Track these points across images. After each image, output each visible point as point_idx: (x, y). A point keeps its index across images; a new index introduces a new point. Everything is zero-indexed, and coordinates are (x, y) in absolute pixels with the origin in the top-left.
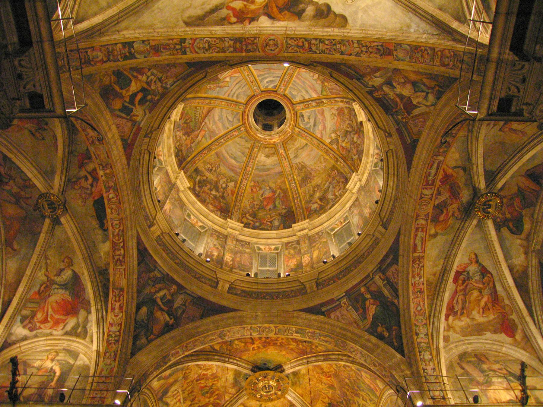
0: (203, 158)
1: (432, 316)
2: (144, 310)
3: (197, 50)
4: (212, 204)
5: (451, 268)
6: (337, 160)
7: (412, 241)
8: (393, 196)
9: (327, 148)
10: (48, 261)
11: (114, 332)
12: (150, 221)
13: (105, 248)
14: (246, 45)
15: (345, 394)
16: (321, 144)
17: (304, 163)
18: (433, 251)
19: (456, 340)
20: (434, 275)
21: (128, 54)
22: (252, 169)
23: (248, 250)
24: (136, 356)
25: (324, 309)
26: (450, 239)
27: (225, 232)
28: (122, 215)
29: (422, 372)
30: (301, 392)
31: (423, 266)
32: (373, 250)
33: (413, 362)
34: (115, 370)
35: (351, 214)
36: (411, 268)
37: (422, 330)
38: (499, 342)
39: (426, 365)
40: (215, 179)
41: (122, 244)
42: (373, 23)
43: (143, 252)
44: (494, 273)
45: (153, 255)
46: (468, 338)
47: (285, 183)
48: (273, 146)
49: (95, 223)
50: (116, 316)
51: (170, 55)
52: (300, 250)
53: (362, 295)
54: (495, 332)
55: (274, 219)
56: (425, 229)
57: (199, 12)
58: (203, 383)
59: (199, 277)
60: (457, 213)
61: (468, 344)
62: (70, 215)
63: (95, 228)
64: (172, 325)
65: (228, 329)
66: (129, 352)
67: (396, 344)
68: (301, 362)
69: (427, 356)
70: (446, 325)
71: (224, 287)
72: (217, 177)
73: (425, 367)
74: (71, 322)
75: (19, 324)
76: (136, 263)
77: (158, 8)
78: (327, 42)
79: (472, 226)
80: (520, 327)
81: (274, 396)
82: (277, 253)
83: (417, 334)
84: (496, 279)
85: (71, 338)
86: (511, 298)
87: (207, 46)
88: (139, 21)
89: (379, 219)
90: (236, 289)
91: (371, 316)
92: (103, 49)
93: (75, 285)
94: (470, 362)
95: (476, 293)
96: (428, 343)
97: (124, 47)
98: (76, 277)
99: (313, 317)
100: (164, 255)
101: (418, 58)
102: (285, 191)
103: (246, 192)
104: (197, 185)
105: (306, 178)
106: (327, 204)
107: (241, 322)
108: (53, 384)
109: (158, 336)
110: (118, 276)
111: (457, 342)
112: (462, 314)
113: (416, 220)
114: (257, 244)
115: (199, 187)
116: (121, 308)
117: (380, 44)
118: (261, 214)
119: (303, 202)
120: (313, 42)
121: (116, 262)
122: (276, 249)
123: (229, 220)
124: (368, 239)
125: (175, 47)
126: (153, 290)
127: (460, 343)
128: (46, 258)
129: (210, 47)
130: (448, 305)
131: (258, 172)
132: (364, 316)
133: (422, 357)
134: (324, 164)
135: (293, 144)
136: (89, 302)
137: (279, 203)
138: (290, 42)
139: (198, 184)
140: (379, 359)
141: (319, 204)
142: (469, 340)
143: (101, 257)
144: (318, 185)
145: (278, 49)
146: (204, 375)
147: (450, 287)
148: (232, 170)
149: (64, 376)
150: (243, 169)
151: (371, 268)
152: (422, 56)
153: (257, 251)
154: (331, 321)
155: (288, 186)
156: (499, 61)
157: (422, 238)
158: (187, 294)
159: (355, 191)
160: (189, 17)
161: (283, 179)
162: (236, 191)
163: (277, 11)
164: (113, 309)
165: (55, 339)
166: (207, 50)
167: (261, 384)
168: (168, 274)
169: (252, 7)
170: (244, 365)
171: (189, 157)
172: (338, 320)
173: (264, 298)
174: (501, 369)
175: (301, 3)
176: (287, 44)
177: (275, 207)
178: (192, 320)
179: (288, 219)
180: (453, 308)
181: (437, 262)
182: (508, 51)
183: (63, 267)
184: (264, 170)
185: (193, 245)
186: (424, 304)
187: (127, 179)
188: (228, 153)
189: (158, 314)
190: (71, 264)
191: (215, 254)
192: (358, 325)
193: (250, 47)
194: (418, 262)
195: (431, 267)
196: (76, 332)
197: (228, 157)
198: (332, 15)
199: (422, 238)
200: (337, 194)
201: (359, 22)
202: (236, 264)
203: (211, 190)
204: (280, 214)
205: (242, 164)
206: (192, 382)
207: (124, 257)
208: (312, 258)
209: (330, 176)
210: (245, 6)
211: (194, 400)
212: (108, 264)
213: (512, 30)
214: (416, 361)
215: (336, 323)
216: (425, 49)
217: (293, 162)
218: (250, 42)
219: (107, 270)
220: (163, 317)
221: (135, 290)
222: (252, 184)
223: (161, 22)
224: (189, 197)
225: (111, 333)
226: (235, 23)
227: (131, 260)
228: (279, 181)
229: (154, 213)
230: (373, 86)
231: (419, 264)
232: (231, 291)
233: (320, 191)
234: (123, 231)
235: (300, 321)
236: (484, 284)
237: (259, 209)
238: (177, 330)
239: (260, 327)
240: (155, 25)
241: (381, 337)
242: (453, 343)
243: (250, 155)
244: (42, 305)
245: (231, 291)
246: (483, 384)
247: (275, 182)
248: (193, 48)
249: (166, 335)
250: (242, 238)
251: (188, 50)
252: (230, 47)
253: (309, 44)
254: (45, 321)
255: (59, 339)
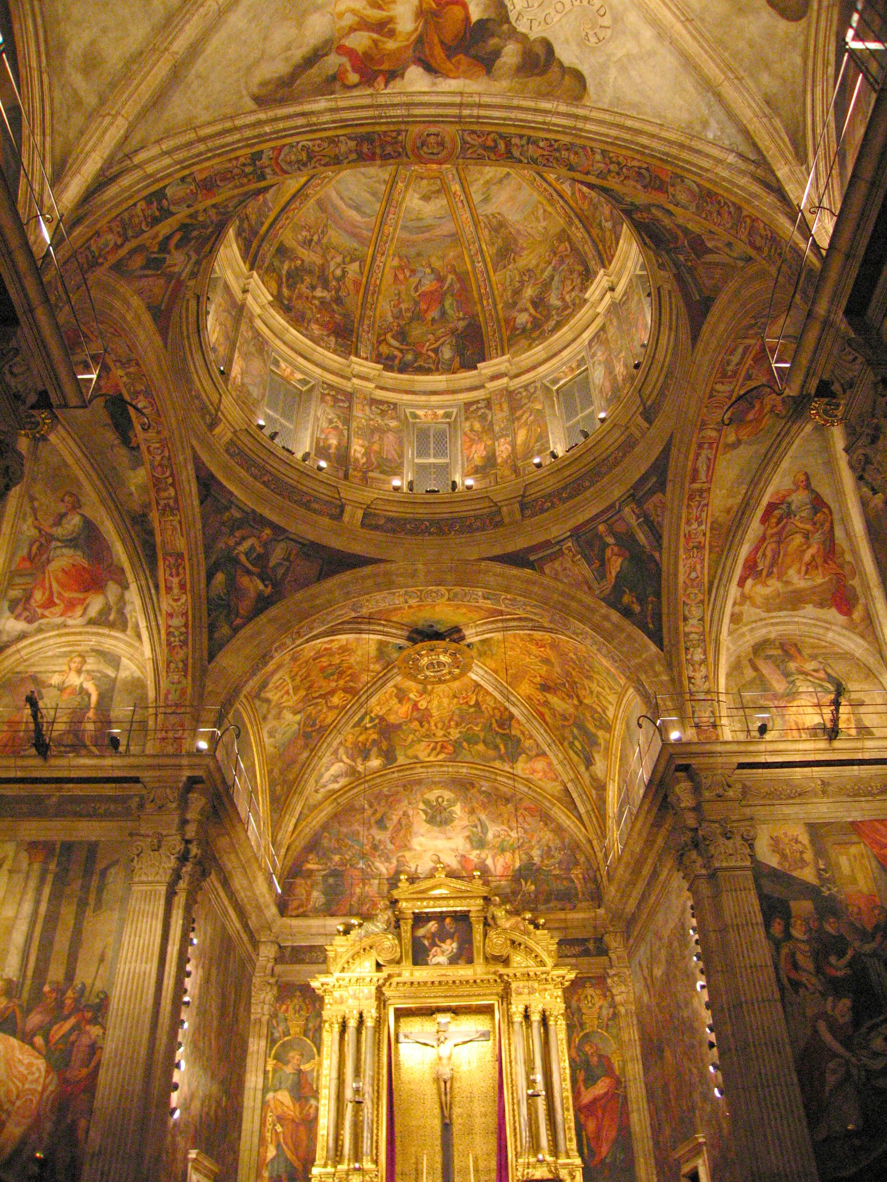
0: (292, 219)
1: (716, 582)
2: (220, 577)
3: (285, 167)
4: (317, 321)
5: (758, 503)
6: (570, 223)
7: (690, 464)
8: (666, 364)
9: (551, 190)
10: (36, 504)
11: (177, 628)
12: (211, 415)
13: (137, 478)
14: (382, 146)
15: (568, 674)
16: (538, 178)
17: (502, 216)
18: (728, 472)
19: (754, 618)
20: (728, 511)
21: (157, 213)
22: (395, 230)
23: (393, 424)
24: (217, 659)
25: (532, 558)
26: (763, 450)
27: (347, 385)
28: (166, 433)
29: (686, 682)
30: (493, 666)
31: (707, 505)
32: (624, 456)
33: (675, 664)
34: (189, 690)
35: (592, 358)
36: (684, 507)
37: (696, 612)
38: (825, 621)
39: (694, 671)
40: (319, 261)
41: (170, 480)
42: (637, 98)
43: (207, 484)
44: (834, 506)
45: (225, 483)
46: (774, 614)
47: (463, 259)
48: (438, 174)
49: (111, 436)
50: (176, 600)
51: (236, 187)
52: (491, 424)
53: (601, 538)
54: (821, 605)
55: (442, 344)
56: (715, 445)
57: (279, 68)
58: (325, 661)
59: (307, 502)
60: (780, 408)
61: (773, 624)
62: (64, 427)
63: (112, 446)
64: (270, 596)
65: (367, 597)
66: (205, 654)
67: (651, 626)
68: (494, 626)
69: (698, 656)
70: (738, 594)
71: (353, 516)
72: (324, 256)
73: (691, 674)
74: (96, 604)
75: (8, 614)
76: (196, 503)
77: (199, 76)
78: (541, 144)
79: (802, 434)
80: (862, 601)
81: (448, 677)
82: (449, 423)
83: (685, 619)
84: (836, 517)
85: (100, 631)
86: (855, 552)
87: (304, 157)
88: (166, 115)
89: (639, 400)
90: (375, 515)
91: (614, 574)
92: (113, 225)
93: (90, 539)
94: (768, 657)
95: (798, 539)
96: (703, 633)
97: (149, 203)
98: (89, 526)
99: (515, 571)
100: (243, 473)
101: (711, 214)
102: (462, 278)
103: (384, 282)
104: (284, 285)
105: (507, 252)
106: (548, 317)
107: (388, 584)
108: (91, 714)
109: (250, 619)
110: (169, 532)
111: (755, 621)
112: (770, 574)
113: (701, 430)
114: (412, 406)
115: (289, 287)
116: (182, 587)
117: (645, 166)
118: (417, 332)
119: (500, 306)
120: (515, 141)
121: (164, 510)
122: (447, 415)
123: (353, 358)
124: (617, 433)
125: (243, 171)
126: (231, 543)
127: (759, 624)
128: (32, 499)
129: (310, 157)
130: (746, 561)
131: (405, 235)
132: (602, 574)
133: (689, 657)
134: (544, 224)
135: (481, 173)
136: (123, 570)
137: (451, 305)
138: (469, 139)
139: (287, 280)
140: (621, 652)
141: (530, 315)
142: (776, 617)
143: (131, 494)
144: (528, 270)
145: (445, 152)
146: (326, 649)
147: (755, 528)
148: (354, 235)
149: (105, 698)
150: (376, 230)
151: (617, 493)
152: (719, 213)
153: (411, 420)
154: (545, 580)
155: (470, 269)
156: (827, 323)
157: (709, 459)
158: (291, 540)
159: (601, 308)
160: (263, 85)
161: (459, 249)
162: (364, 280)
163: (443, 55)
164: (169, 589)
165: (74, 634)
166: (305, 165)
167: (425, 661)
168: (254, 511)
169: (391, 45)
170: (394, 631)
171: (262, 224)
172: (556, 578)
173: (426, 531)
174: (816, 671)
175: (492, 35)
176: (464, 142)
177: (443, 313)
178: (305, 584)
179: (471, 348)
180: (755, 564)
181: (735, 490)
182: (841, 314)
183: (63, 510)
184: (421, 230)
185: (291, 427)
186: (703, 568)
187: (165, 367)
188: (342, 198)
189: (245, 581)
190: (77, 505)
191: (334, 442)
192: (590, 588)
193: (389, 149)
194: (697, 498)
195: (721, 500)
196: (107, 619)
197: (344, 207)
198: (555, 69)
199: (709, 459)
200: (567, 298)
201: (610, 92)
202: (373, 460)
203: (313, 288)
204: (453, 332)
205: (374, 218)
206: (306, 662)
207: (176, 501)
208: (513, 445)
209: (555, 254)
210: (375, 42)
211: (310, 687)
212: (147, 506)
213: (851, 282)
214: (680, 664)
215: (552, 583)
216: (725, 203)
217: (479, 211)
218: (388, 139)
219: (145, 515)
220: (253, 586)
221: (201, 549)
222: (396, 263)
223: (207, 108)
224: (271, 322)
225: (171, 629)
226: (355, 86)
227: (189, 501)
228: (452, 254)
229: (215, 398)
230: (632, 204)
231: (700, 502)
232: (367, 521)
233: (534, 284)
234: (169, 459)
235: (491, 579)
236: (814, 524)
237: (412, 319)
238: (279, 605)
239: (421, 591)
240: (196, 118)
241: (627, 613)
242: (745, 625)
243: (389, 200)
244: (40, 577)
245: (367, 521)
246: (782, 696)
247: (443, 257)
248: (278, 164)
249: (262, 616)
250: (380, 395)
251: (268, 170)
252: (351, 151)
253: (506, 146)
254: (49, 603)
255: (80, 633)
